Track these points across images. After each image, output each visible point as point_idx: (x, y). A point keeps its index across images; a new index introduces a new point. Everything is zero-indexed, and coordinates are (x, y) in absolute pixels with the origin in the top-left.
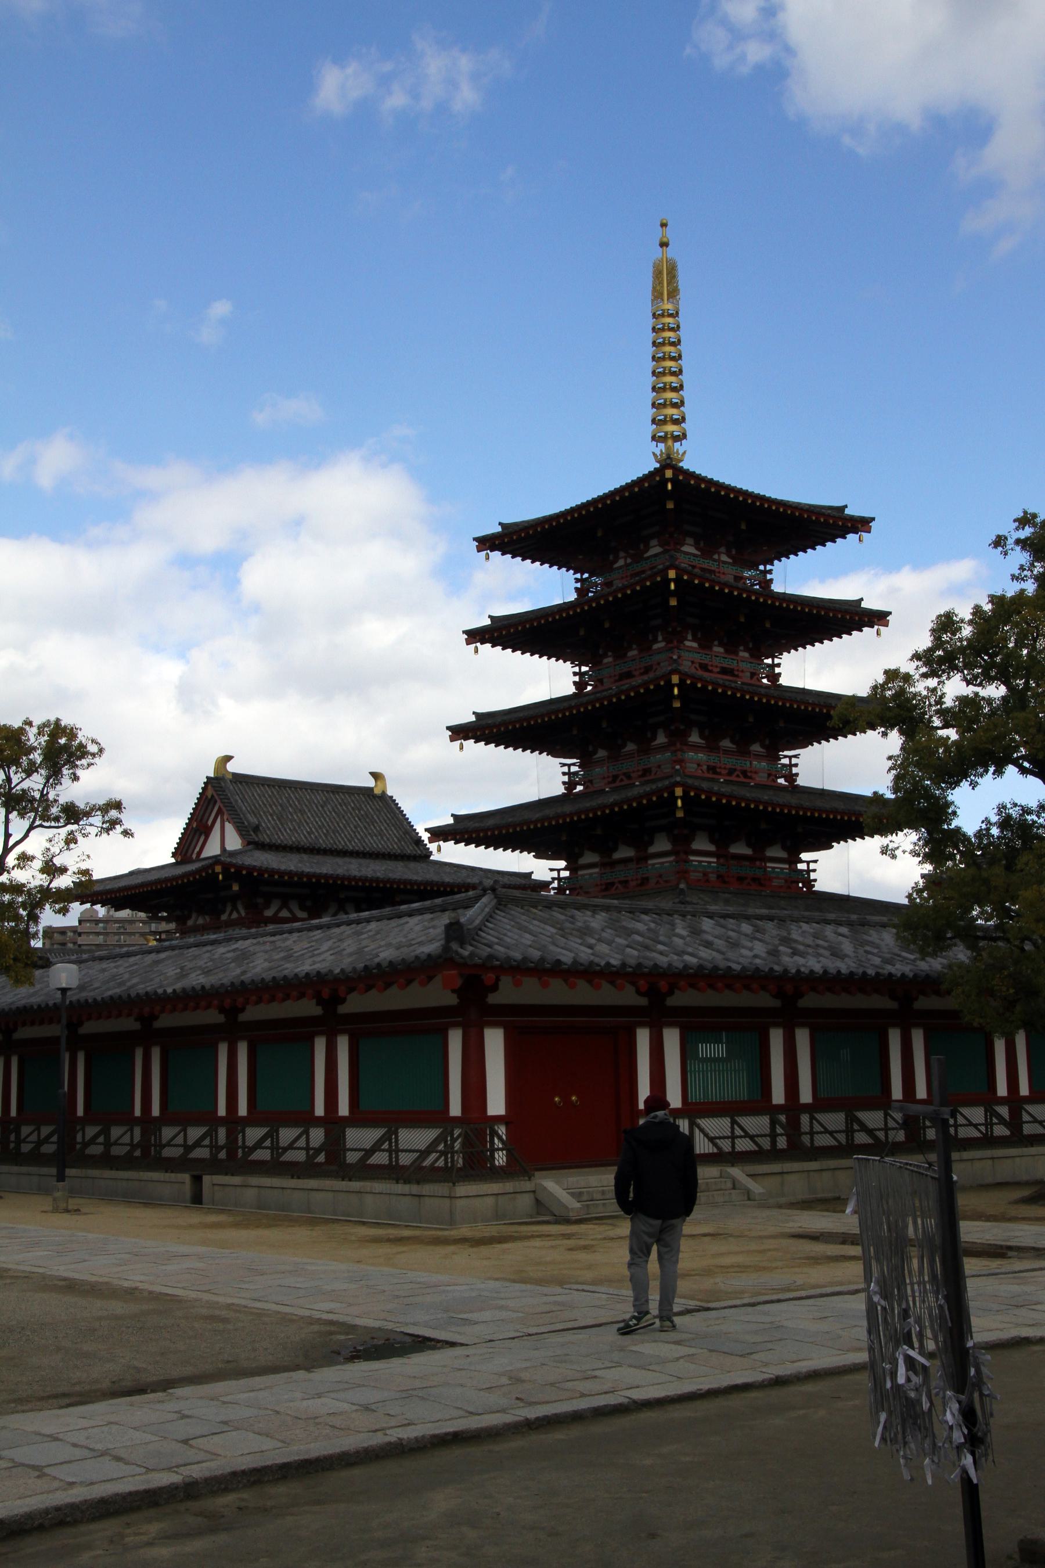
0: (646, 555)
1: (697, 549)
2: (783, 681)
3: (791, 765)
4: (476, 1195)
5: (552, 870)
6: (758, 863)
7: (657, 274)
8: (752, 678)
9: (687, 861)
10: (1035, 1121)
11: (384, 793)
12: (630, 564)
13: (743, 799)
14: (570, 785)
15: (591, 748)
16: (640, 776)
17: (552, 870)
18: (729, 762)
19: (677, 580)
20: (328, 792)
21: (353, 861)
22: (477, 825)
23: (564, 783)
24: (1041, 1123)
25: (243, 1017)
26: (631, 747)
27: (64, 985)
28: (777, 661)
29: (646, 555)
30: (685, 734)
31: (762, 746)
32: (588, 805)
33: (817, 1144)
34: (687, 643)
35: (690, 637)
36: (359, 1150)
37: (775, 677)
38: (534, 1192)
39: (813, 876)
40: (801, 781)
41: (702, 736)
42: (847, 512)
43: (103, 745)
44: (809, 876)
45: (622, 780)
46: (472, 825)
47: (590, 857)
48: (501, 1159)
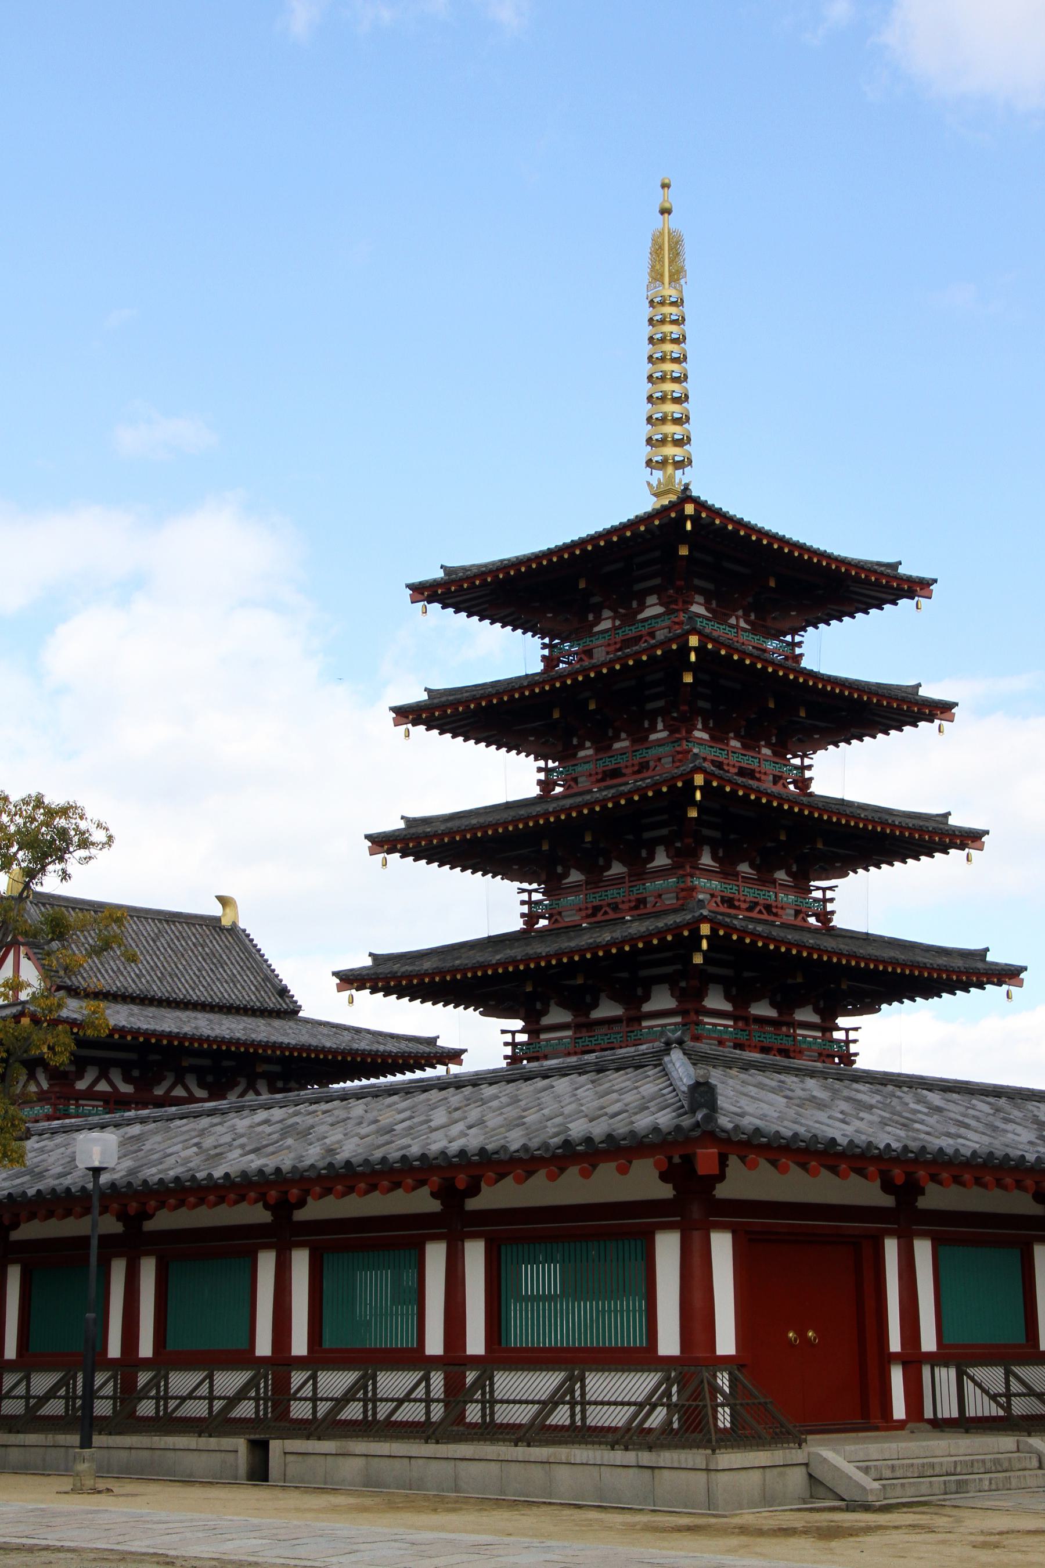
0: (641, 616)
1: (707, 610)
2: (816, 788)
3: (825, 901)
4: (681, 1468)
5: (503, 1032)
6: (784, 1029)
7: (657, 250)
8: (775, 783)
9: (698, 1023)
10: (1031, 1392)
11: (234, 925)
12: (619, 627)
13: (783, 942)
14: (530, 919)
15: (560, 870)
16: (631, 909)
17: (503, 1032)
18: (750, 893)
19: (700, 650)
20: (160, 921)
21: (199, 1015)
22: (409, 968)
23: (523, 915)
24: (1039, 1396)
25: (301, 1215)
26: (617, 869)
27: (97, 1164)
28: (807, 762)
29: (641, 616)
30: (694, 854)
31: (788, 874)
32: (573, 944)
33: (499, 1418)
34: (697, 734)
35: (700, 726)
36: (629, 1404)
37: (804, 784)
38: (807, 1465)
39: (853, 1049)
40: (837, 922)
41: (714, 858)
42: (902, 570)
43: (112, 832)
44: (848, 1047)
45: (606, 913)
46: (397, 968)
47: (557, 1015)
48: (724, 1418)
